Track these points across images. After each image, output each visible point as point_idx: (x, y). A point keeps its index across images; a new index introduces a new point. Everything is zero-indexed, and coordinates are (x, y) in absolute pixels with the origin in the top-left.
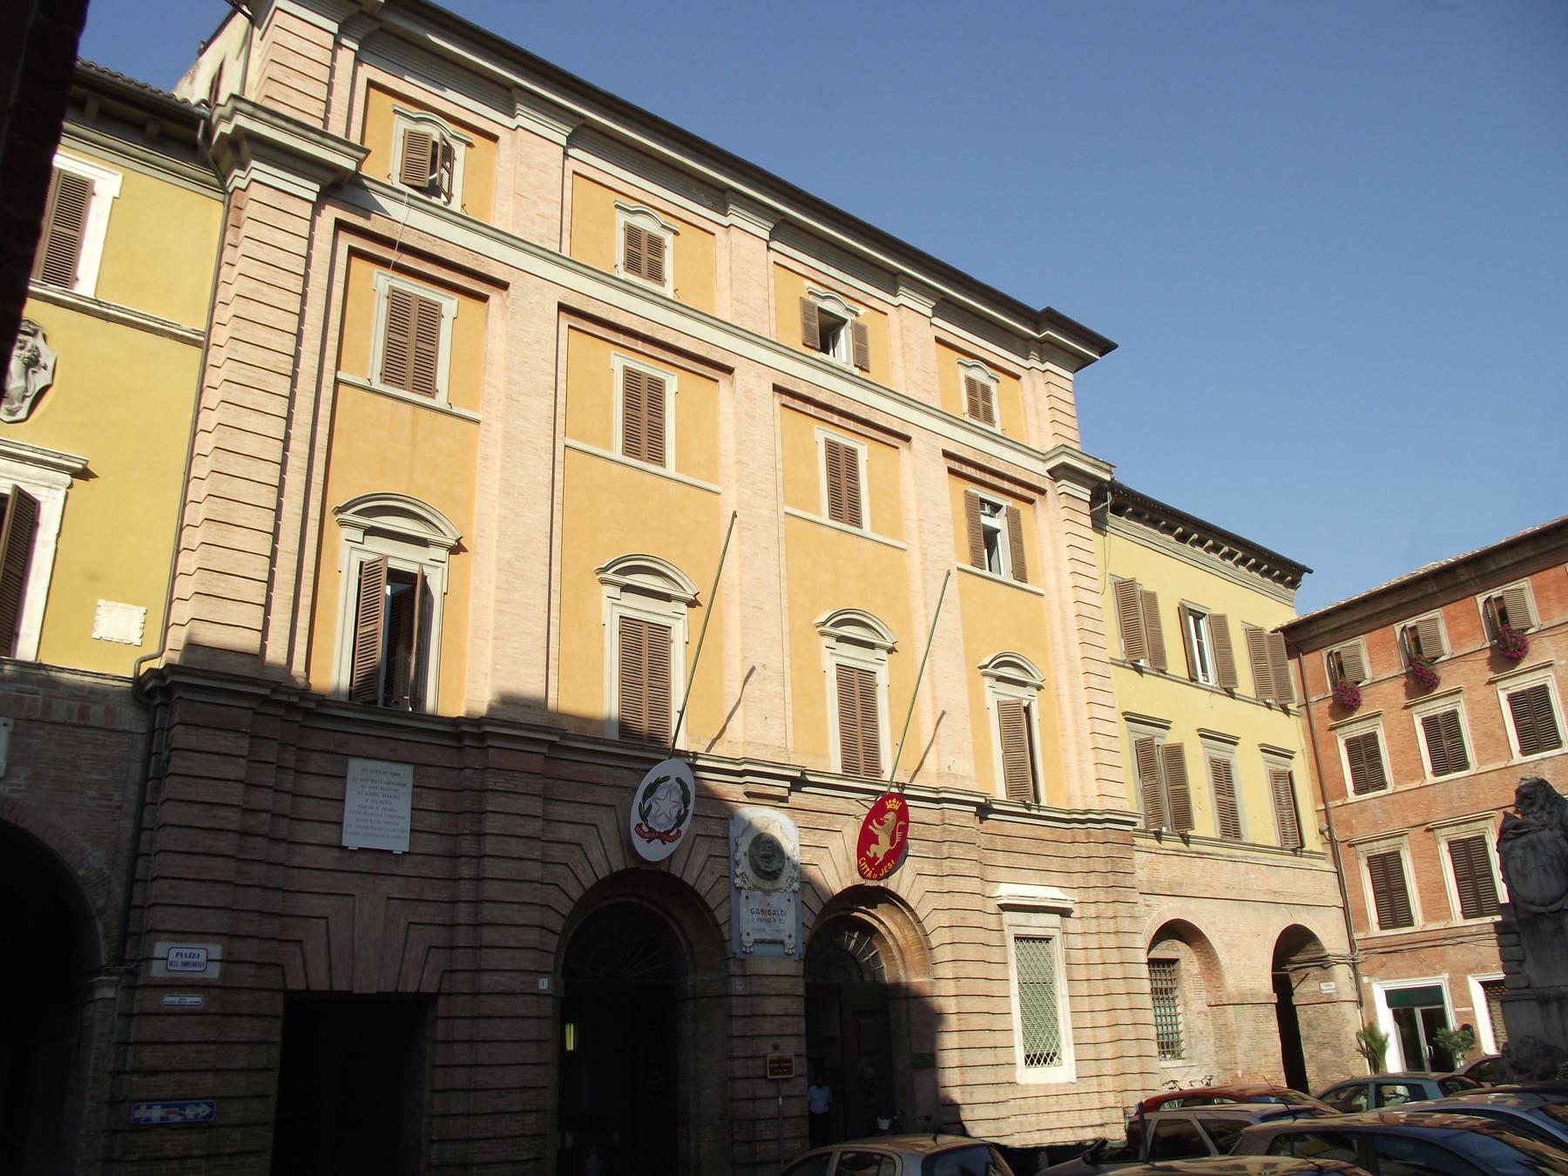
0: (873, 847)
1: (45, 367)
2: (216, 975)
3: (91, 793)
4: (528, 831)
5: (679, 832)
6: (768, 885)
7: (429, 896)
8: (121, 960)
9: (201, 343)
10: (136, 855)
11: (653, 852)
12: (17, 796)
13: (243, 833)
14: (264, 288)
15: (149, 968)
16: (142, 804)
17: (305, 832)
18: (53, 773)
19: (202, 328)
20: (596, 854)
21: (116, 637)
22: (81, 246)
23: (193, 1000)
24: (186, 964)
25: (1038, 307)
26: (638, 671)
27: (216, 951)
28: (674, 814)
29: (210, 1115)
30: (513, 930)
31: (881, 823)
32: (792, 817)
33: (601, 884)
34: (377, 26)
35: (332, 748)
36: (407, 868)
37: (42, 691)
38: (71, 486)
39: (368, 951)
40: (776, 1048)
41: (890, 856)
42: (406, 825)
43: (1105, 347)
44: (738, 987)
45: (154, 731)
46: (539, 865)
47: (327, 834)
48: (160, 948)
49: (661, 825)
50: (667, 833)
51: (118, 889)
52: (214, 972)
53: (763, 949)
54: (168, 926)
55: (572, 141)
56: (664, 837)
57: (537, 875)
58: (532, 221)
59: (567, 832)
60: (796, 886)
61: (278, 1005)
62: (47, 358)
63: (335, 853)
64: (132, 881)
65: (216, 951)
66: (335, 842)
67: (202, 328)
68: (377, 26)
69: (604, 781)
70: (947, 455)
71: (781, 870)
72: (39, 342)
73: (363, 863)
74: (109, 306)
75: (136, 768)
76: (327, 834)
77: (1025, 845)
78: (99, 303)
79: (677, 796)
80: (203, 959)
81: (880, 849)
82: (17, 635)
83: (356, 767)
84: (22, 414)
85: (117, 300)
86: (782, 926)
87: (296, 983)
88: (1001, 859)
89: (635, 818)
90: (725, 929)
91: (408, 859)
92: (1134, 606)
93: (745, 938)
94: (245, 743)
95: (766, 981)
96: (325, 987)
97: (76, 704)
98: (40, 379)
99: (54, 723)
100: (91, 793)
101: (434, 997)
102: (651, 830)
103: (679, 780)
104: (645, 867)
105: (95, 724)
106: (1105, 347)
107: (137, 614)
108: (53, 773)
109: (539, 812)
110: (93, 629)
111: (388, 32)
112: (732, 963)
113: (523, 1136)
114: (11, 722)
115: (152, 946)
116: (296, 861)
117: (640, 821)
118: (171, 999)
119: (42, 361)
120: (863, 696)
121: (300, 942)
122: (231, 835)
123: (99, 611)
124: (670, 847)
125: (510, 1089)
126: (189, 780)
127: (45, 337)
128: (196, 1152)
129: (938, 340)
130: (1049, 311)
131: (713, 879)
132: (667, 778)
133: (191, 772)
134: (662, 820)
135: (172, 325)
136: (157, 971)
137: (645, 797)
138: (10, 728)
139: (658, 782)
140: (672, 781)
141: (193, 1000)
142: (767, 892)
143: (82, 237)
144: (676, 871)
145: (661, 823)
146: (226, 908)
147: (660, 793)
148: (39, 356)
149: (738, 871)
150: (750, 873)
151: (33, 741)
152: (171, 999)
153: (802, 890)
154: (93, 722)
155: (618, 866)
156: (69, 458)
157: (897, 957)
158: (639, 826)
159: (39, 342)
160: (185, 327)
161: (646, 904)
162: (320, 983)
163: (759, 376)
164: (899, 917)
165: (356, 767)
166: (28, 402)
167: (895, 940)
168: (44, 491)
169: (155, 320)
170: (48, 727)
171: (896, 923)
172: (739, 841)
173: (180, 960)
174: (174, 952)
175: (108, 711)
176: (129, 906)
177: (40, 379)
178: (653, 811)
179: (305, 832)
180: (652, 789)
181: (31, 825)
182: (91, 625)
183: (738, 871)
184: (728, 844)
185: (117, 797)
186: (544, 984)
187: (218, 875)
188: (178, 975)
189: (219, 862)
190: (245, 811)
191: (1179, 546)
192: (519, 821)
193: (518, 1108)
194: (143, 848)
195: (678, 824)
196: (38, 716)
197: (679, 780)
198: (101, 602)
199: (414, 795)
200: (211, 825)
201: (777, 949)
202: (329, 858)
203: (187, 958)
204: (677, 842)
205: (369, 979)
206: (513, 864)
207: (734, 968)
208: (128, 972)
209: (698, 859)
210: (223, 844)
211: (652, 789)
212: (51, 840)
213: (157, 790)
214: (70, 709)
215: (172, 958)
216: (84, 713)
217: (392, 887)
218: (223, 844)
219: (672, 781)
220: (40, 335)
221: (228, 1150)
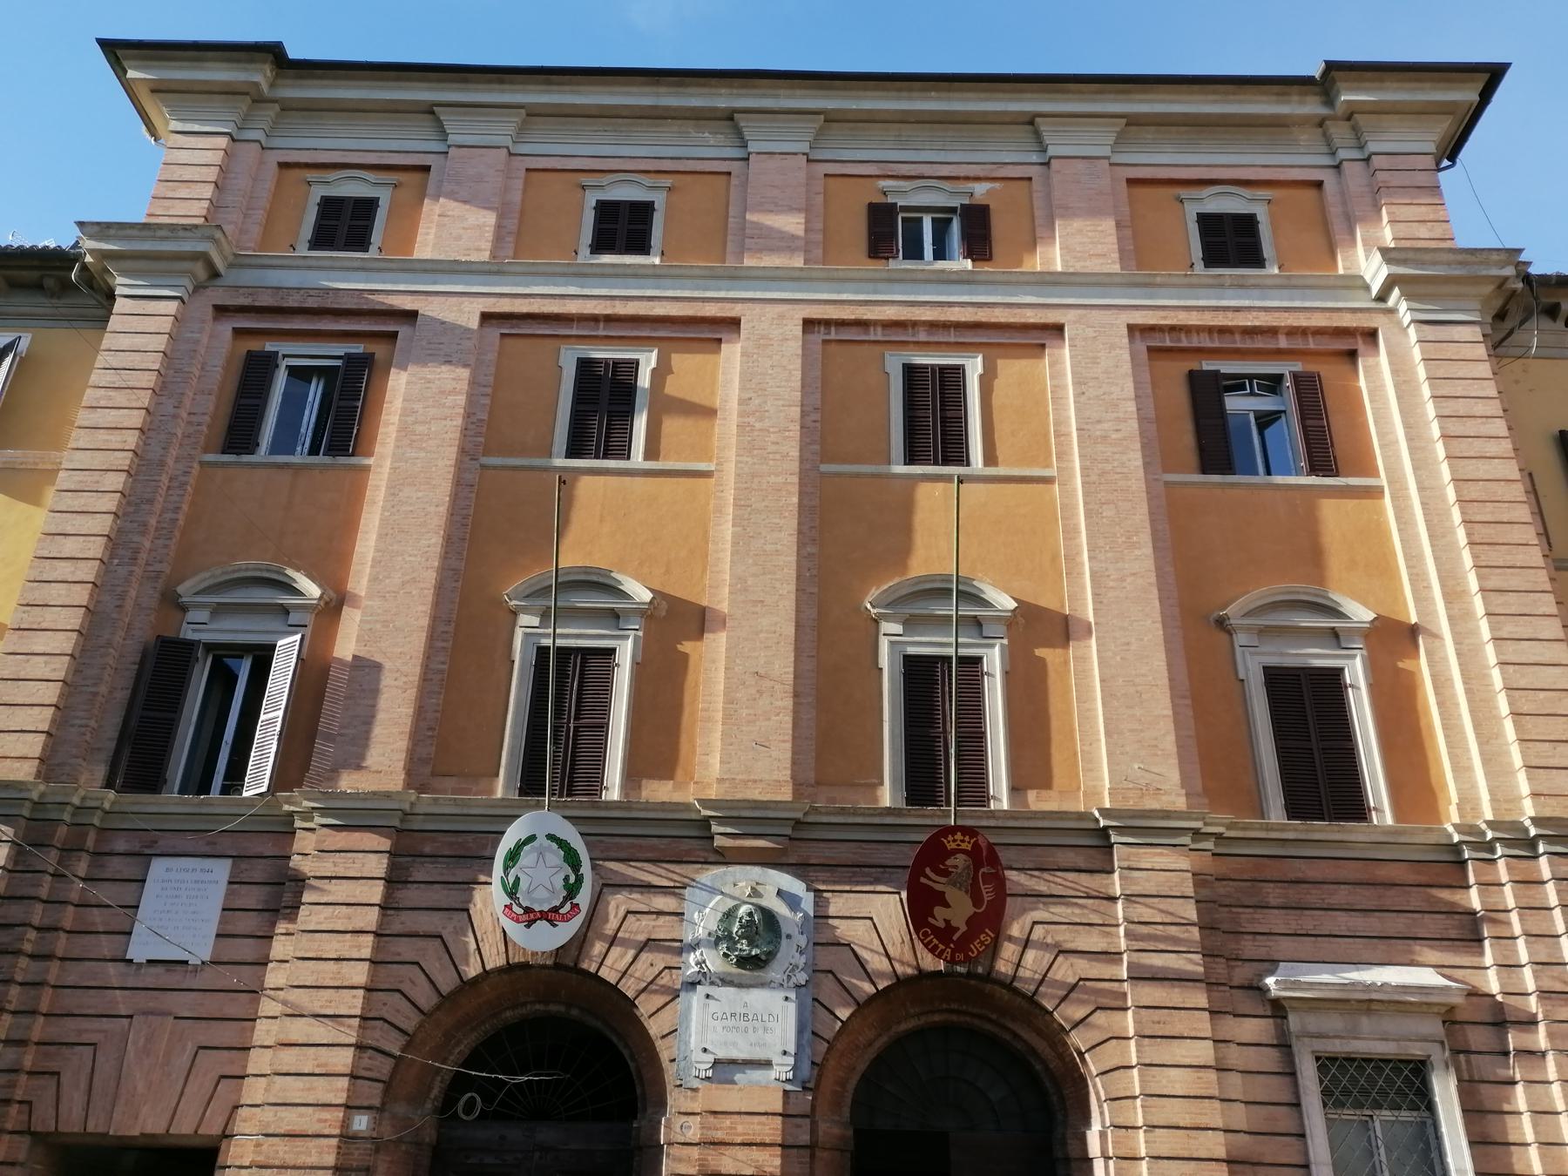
5: (575, 906)
28: (559, 883)
31: (945, 873)
34: (277, 106)
35: (137, 849)
36: (207, 979)
41: (975, 924)
43: (1493, 74)
49: (541, 902)
50: (555, 910)
55: (1120, 141)
56: (551, 916)
68: (1124, 121)
79: (556, 856)
81: (958, 910)
86: (768, 1037)
95: (727, 1122)
102: (528, 910)
103: (551, 837)
114: (793, 995)
117: (508, 901)
121: (58, 1074)
130: (1331, 67)
132: (532, 838)
134: (541, 894)
137: (506, 869)
139: (520, 846)
140: (542, 840)
147: (527, 857)
158: (509, 907)
167: (1044, 1062)
178: (523, 885)
180: (513, 856)
197: (551, 837)
219: (542, 840)
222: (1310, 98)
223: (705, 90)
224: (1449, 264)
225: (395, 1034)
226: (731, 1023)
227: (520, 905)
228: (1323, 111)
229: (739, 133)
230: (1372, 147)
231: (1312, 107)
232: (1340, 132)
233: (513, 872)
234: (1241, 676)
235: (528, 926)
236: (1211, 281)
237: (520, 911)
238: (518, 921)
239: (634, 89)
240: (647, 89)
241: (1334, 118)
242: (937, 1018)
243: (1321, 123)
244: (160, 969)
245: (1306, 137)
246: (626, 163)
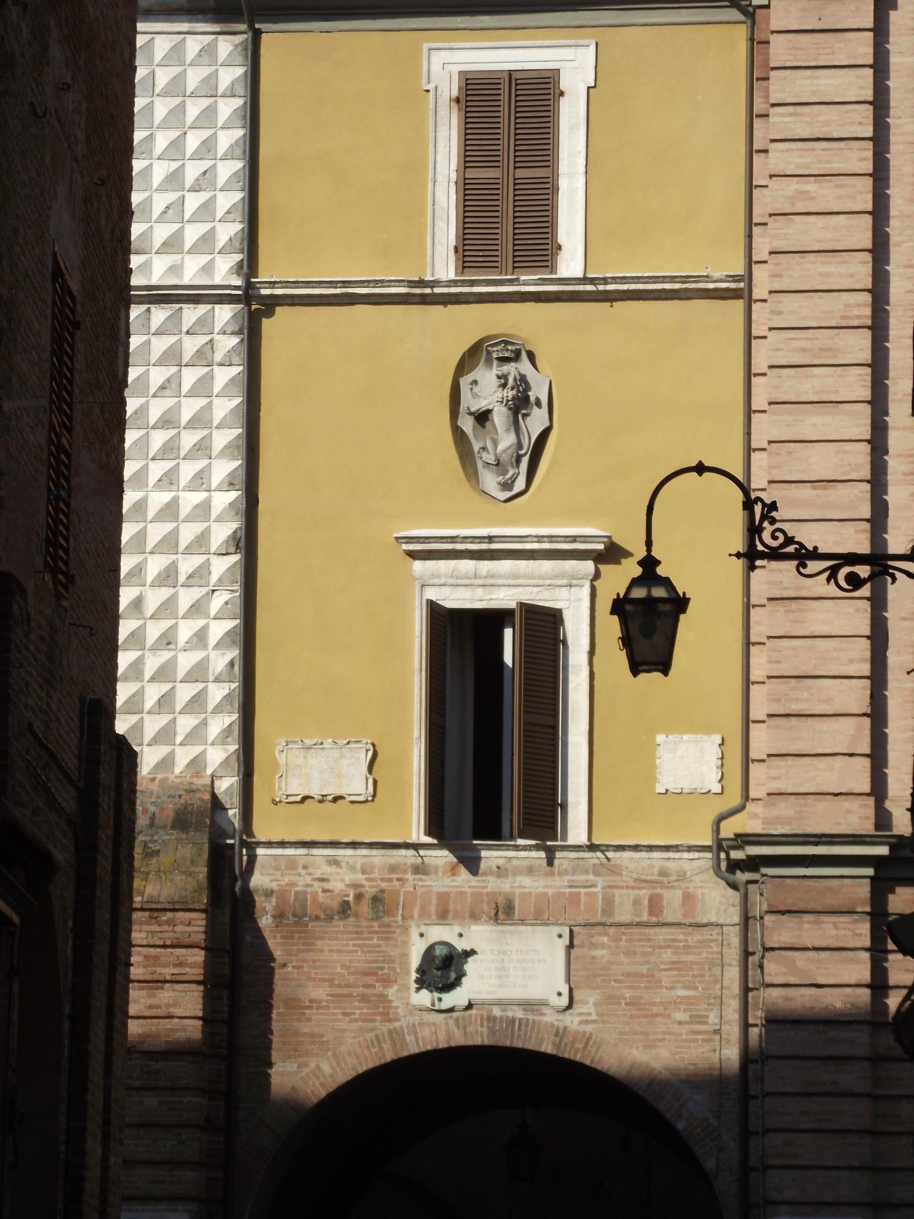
1: (538, 403)
3: (681, 1016)
9: (740, 292)
12: (588, 1028)
14: (811, 186)
18: (628, 994)
19: (740, 271)
21: (687, 786)
22: (555, 190)
37: (600, 882)
38: (597, 575)
62: (539, 391)
64: (745, 1135)
67: (740, 271)
72: (525, 366)
74: (605, 281)
78: (592, 281)
82: (849, 553)
84: (520, 485)
85: (618, 267)
97: (644, 894)
99: (619, 925)
100: (681, 1016)
105: (670, 919)
107: (710, 746)
108: (628, 994)
119: (532, 396)
123: (660, 752)
127: (531, 357)
135: (698, 279)
143: (555, 175)
146: (862, 1168)
148: (528, 388)
154: (669, 916)
156: (585, 538)
159: (525, 366)
160: (717, 275)
166: (525, 461)
168: (564, 593)
169: (672, 279)
170: (612, 931)
175: (688, 898)
176: (745, 1168)
177: (536, 422)
182: (650, 774)
185: (713, 1018)
196: (599, 918)
198: (660, 738)
200: (830, 1052)
214: (636, 902)
216: (655, 904)
220: (524, 355)
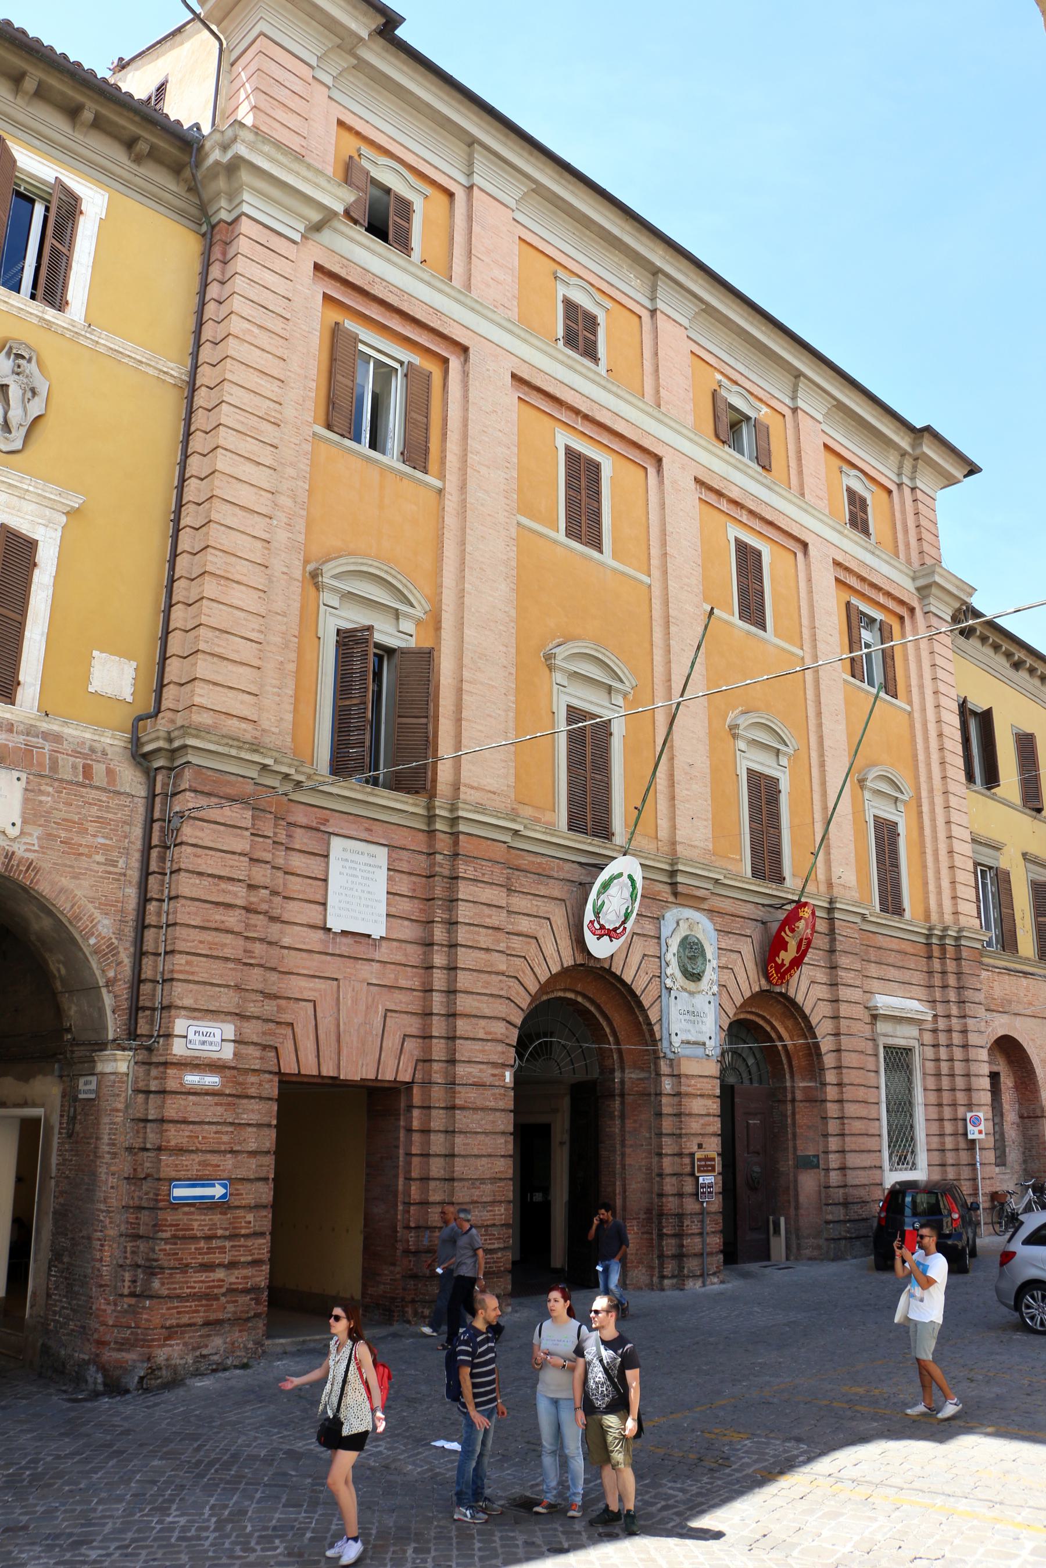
0: (782, 953)
2: (230, 1056)
3: (99, 858)
4: (494, 921)
6: (691, 986)
7: (403, 983)
8: (132, 1034)
10: (141, 927)
11: (600, 948)
13: (247, 909)
15: (168, 1046)
16: (146, 873)
17: (294, 911)
20: (549, 949)
23: (212, 1080)
24: (204, 1043)
25: (919, 425)
26: (582, 763)
27: (229, 1030)
29: (224, 1196)
30: (482, 1023)
31: (792, 931)
32: (711, 919)
33: (554, 978)
35: (314, 824)
36: (384, 953)
37: (47, 746)
39: (359, 1040)
40: (700, 1146)
42: (382, 909)
43: (973, 470)
44: (667, 1085)
45: (155, 796)
46: (504, 958)
47: (312, 914)
48: (180, 1025)
49: (611, 922)
50: (615, 929)
51: (126, 958)
52: (227, 1053)
53: (688, 1051)
54: (188, 1002)
56: (612, 934)
57: (503, 967)
58: (488, 286)
59: (525, 925)
60: (715, 989)
61: (272, 1089)
63: (320, 934)
65: (229, 1030)
66: (320, 923)
69: (555, 875)
70: (837, 564)
71: (703, 972)
73: (345, 946)
75: (137, 832)
76: (312, 914)
77: (892, 958)
79: (627, 894)
80: (218, 1039)
83: (337, 844)
84: (18, 445)
86: (704, 1028)
87: (289, 1066)
88: (873, 970)
89: (589, 915)
90: (656, 1028)
91: (384, 944)
92: (977, 726)
93: (674, 1038)
94: (249, 814)
96: (315, 1073)
98: (36, 408)
100: (99, 858)
101: (409, 1086)
102: (602, 927)
103: (630, 877)
104: (592, 963)
106: (973, 470)
109: (503, 903)
110: (88, 682)
111: (361, 66)
112: (662, 1063)
113: (494, 1225)
114: (24, 777)
115: (171, 1022)
116: (286, 941)
117: (593, 918)
118: (192, 1079)
120: (768, 803)
122: (238, 912)
124: (617, 943)
125: (482, 1181)
126: (199, 851)
128: (220, 1232)
129: (826, 446)
130: (928, 429)
131: (647, 978)
132: (621, 875)
133: (200, 843)
134: (611, 917)
136: (178, 1049)
138: (23, 783)
139: (613, 878)
141: (212, 1080)
142: (691, 994)
144: (617, 969)
145: (610, 920)
147: (613, 890)
149: (669, 971)
150: (678, 974)
151: (43, 798)
152: (192, 1079)
153: (720, 992)
155: (568, 962)
157: (785, 1061)
158: (592, 922)
161: (580, 999)
162: (309, 1068)
163: (683, 468)
164: (790, 1023)
165: (337, 844)
171: (786, 1028)
172: (670, 941)
173: (198, 1038)
174: (192, 1030)
176: (137, 980)
179: (294, 911)
180: (606, 886)
181: (44, 887)
183: (669, 971)
184: (659, 944)
185: (121, 863)
186: (508, 1077)
187: (228, 952)
188: (197, 1054)
189: (228, 939)
190: (251, 887)
191: (1011, 672)
192: (487, 911)
193: (489, 1199)
194: (151, 919)
195: (624, 922)
197: (630, 877)
199: (390, 879)
201: (699, 1051)
202: (314, 939)
203: (202, 1037)
204: (623, 938)
205: (356, 1068)
206: (482, 955)
207: (664, 1068)
208: (142, 1047)
209: (635, 959)
210: (232, 919)
211: (606, 886)
212: (63, 904)
213: (162, 859)
215: (191, 1036)
217: (369, 972)
218: (232, 919)
221: (243, 1232)
222: (907, 438)
223: (652, 245)
224: (957, 587)
225: (468, 1011)
226: (687, 1017)
227: (599, 923)
228: (909, 449)
229: (654, 289)
230: (919, 484)
231: (904, 442)
232: (908, 464)
233: (602, 897)
234: (555, 710)
235: (598, 939)
236: (565, 359)
237: (597, 926)
238: (594, 934)
239: (549, 171)
240: (618, 221)
241: (910, 454)
242: (570, 995)
243: (904, 454)
244: (349, 940)
245: (893, 458)
246: (758, 392)
